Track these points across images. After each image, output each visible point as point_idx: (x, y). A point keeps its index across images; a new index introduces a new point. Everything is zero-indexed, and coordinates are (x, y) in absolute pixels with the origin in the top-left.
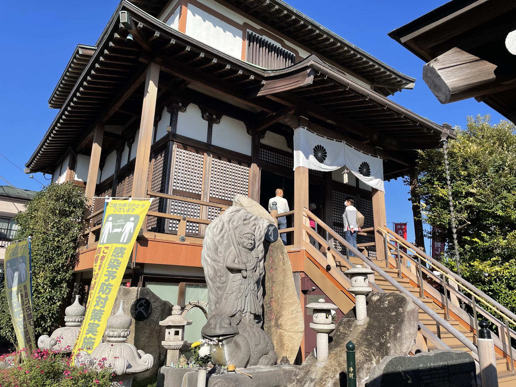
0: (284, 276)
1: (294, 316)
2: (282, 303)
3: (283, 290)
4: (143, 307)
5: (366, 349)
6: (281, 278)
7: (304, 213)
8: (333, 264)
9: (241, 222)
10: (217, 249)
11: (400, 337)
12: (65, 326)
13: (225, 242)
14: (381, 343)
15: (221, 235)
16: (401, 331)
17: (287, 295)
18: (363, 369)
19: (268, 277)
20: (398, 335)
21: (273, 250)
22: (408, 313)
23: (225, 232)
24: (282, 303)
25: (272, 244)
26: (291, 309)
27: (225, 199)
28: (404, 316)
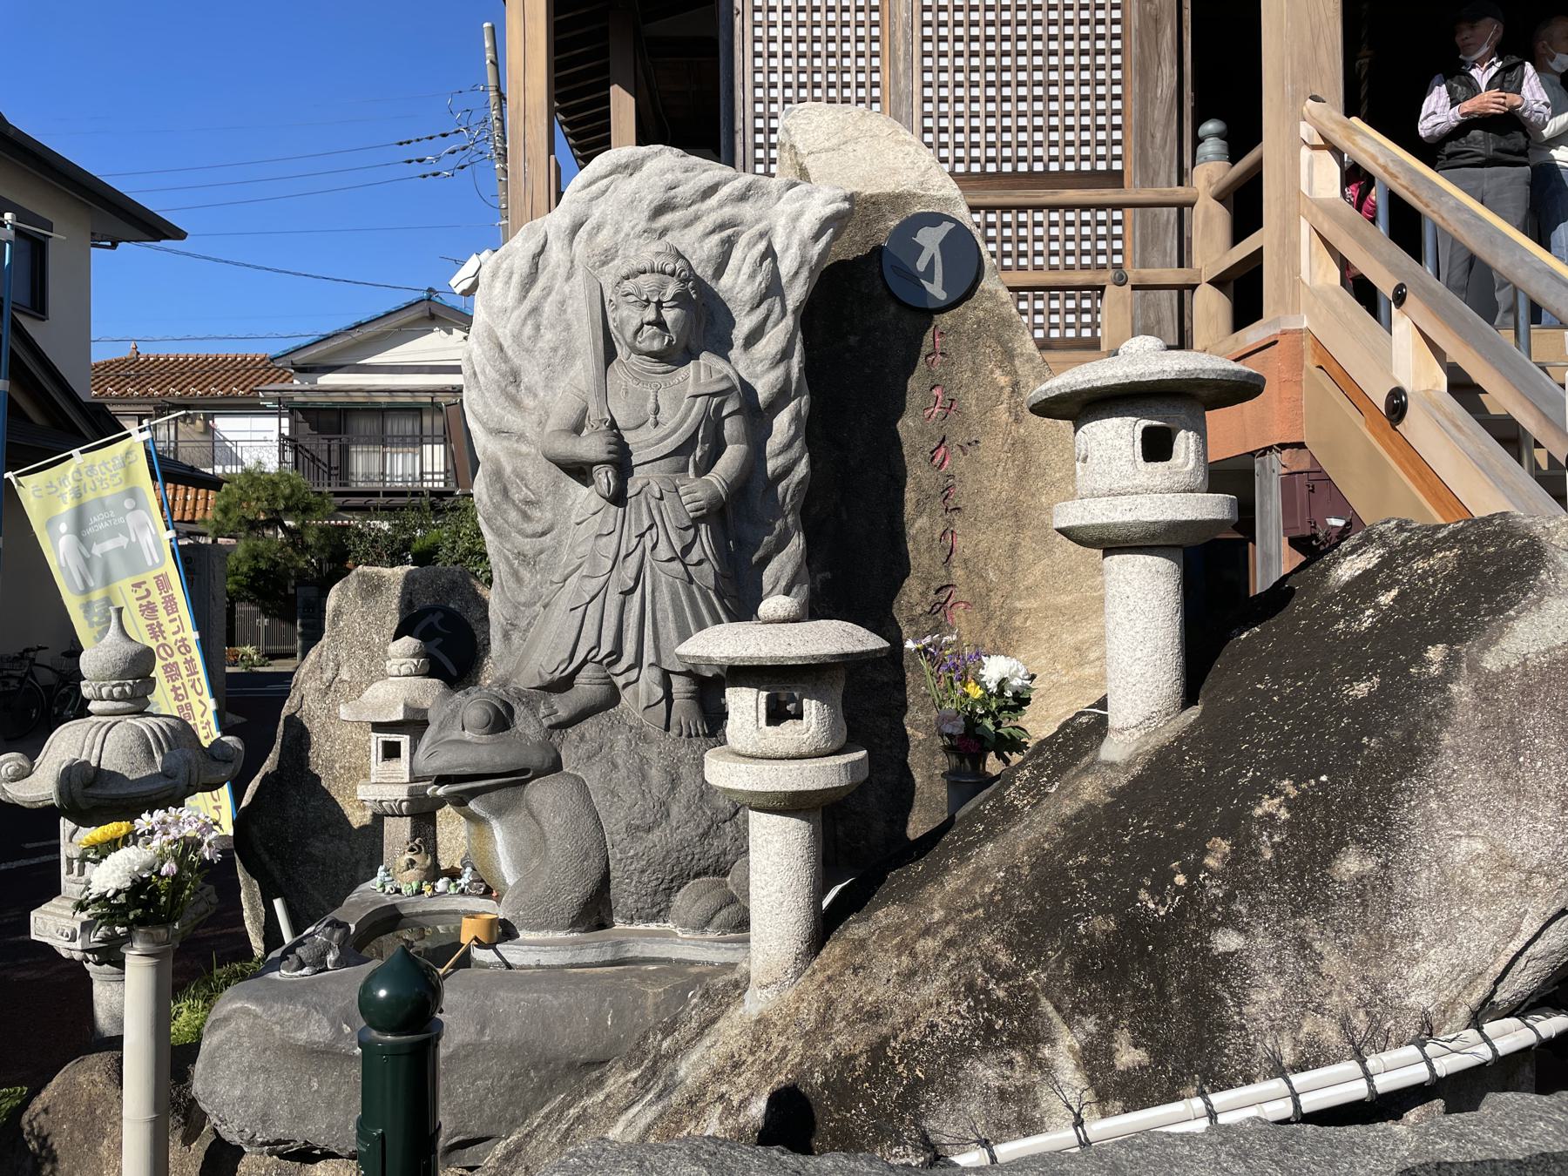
0: (1022, 475)
1: (1088, 671)
2: (1013, 612)
3: (1014, 547)
4: (439, 640)
5: (1003, 958)
6: (1000, 486)
7: (1306, 130)
8: (1421, 377)
9: (640, 219)
10: (515, 376)
11: (1362, 886)
12: (90, 714)
13: (548, 336)
14: (1132, 924)
15: (527, 305)
16: (1382, 832)
17: (1037, 570)
18: (952, 1091)
19: (919, 488)
20: (1351, 864)
21: (950, 347)
22: (1489, 686)
23: (548, 291)
24: (1013, 612)
25: (943, 321)
26: (1069, 639)
27: (1078, 171)
28: (1442, 714)
